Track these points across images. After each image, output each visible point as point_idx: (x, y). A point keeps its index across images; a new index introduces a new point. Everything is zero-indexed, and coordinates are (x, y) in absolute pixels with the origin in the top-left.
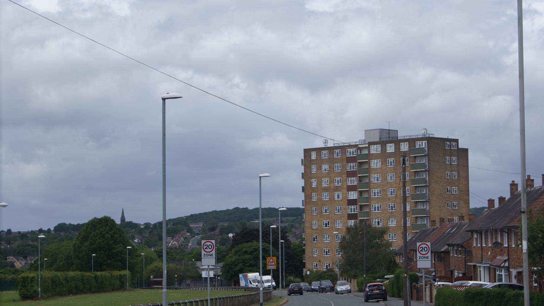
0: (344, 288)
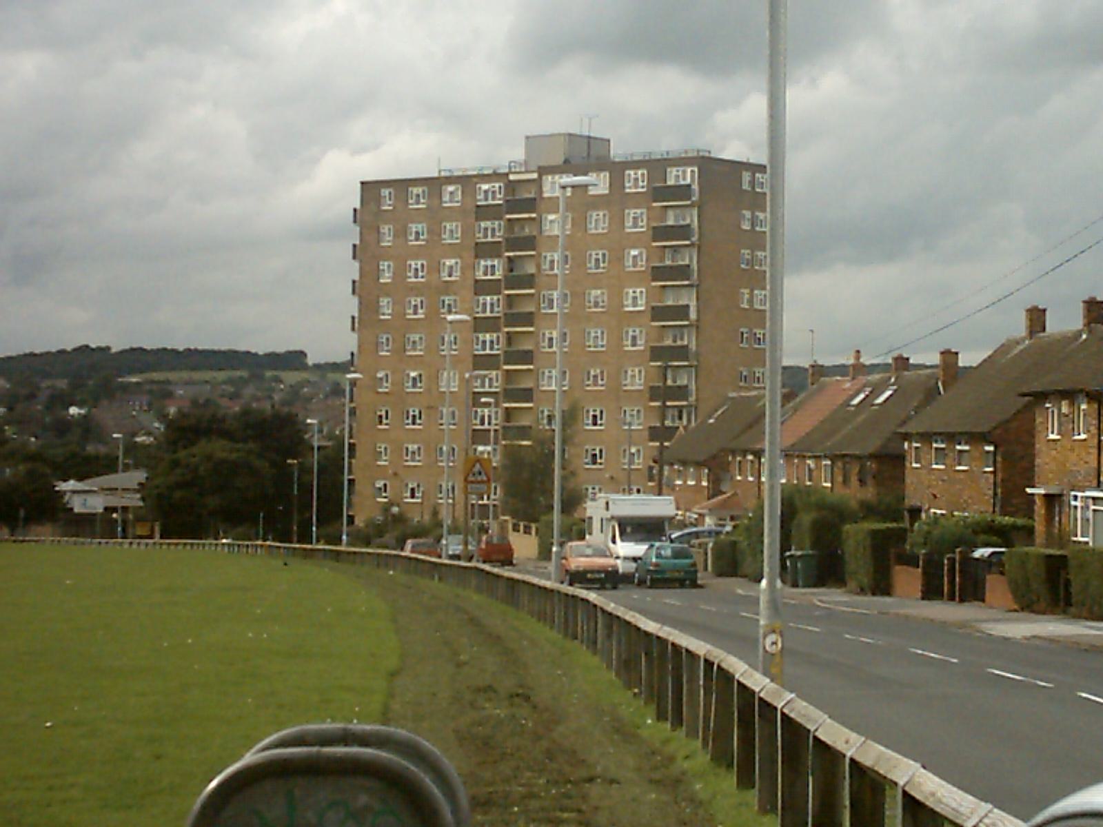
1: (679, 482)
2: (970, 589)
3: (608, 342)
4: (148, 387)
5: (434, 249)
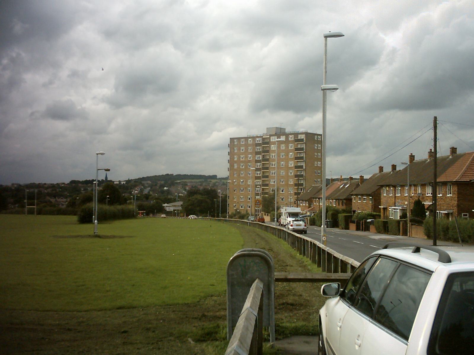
0: (329, 223)
1: (301, 205)
2: (367, 228)
3: (285, 173)
4: (181, 183)
5: (246, 153)
